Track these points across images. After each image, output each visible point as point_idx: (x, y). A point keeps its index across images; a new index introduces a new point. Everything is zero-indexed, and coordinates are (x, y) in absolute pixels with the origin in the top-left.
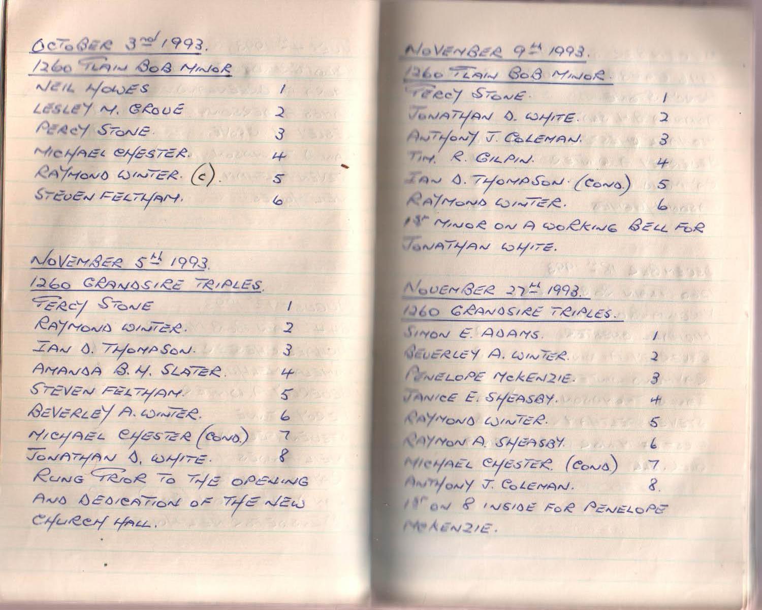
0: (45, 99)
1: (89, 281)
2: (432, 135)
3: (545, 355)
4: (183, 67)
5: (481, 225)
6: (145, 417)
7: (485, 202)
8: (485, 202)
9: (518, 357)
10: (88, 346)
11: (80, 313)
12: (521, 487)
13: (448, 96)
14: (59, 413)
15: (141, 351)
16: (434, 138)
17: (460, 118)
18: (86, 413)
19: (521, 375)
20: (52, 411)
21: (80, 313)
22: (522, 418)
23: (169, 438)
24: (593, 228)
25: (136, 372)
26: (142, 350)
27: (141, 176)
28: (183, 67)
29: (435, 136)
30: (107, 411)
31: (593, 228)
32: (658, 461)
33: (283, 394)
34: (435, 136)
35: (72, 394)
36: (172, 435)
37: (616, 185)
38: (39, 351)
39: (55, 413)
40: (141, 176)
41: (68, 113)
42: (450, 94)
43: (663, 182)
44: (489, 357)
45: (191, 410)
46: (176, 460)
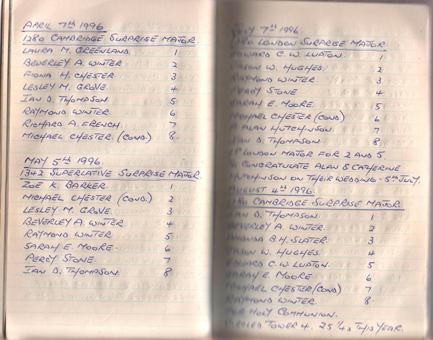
0: (30, 81)
1: (84, 210)
2: (298, 300)
3: (310, 227)
4: (283, 153)
5: (303, 104)
6: (338, 180)
7: (65, 112)
8: (65, 112)
9: (92, 224)
10: (50, 98)
11: (368, 172)
12: (40, 88)
13: (253, 92)
14: (105, 174)
15: (371, 239)
16: (365, 168)
17: (367, 169)
18: (99, 210)
19: (54, 183)
20: (38, 221)
21: (368, 172)
22: (97, 233)
23: (109, 64)
24: (386, 169)
25: (65, 101)
26: (289, 141)
27: (87, 113)
28: (283, 153)
29: (365, 167)
30: (55, 248)
31: (386, 169)
32: (23, 52)
33: (167, 236)
34: (365, 167)
35: (87, 78)
36: (300, 115)
37: (62, 112)
38: (24, 101)
39: (103, 173)
40: (87, 113)
41: (25, 89)
42: (49, 259)
43: (387, 178)
44: (319, 155)
45: (322, 239)
46: (44, 198)
